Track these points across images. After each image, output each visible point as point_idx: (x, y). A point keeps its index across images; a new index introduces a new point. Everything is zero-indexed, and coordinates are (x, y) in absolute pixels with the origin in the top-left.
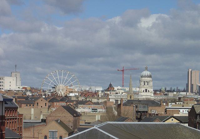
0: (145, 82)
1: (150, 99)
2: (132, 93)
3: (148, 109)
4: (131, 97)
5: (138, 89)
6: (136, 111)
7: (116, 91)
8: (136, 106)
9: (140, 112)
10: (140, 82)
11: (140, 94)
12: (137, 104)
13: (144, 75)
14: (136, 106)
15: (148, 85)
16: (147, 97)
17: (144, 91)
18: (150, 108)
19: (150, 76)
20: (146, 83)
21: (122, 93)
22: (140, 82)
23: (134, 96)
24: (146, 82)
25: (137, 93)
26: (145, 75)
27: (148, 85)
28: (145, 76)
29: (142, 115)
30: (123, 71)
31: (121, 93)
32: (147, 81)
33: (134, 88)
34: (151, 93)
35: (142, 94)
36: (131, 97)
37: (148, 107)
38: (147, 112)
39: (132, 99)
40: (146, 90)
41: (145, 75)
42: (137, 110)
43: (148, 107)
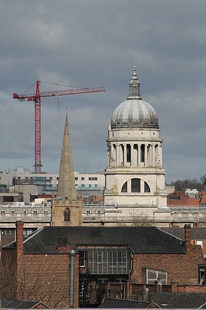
0: (129, 146)
1: (153, 222)
2: (74, 195)
3: (129, 265)
4: (67, 216)
5: (101, 180)
6: (81, 276)
7: (7, 191)
8: (81, 253)
9: (96, 278)
10: (109, 150)
11: (110, 203)
12: (86, 245)
13: (125, 118)
14: (81, 253)
15: (143, 160)
16: (138, 212)
17: (125, 188)
18: (139, 261)
19: (153, 124)
20: (134, 152)
21: (33, 198)
22: (110, 147)
23: (80, 213)
24: (136, 146)
25: (94, 198)
26: (130, 120)
27: (143, 160)
28: (131, 124)
29: (104, 291)
30: (36, 98)
31: (27, 197)
32: (139, 144)
33: (87, 177)
34: (156, 194)
35: (119, 200)
36: (67, 216)
37: (130, 259)
38: (126, 277)
39: (74, 223)
40: (136, 184)
41: (130, 120)
42: (84, 272)
43: (130, 259)
